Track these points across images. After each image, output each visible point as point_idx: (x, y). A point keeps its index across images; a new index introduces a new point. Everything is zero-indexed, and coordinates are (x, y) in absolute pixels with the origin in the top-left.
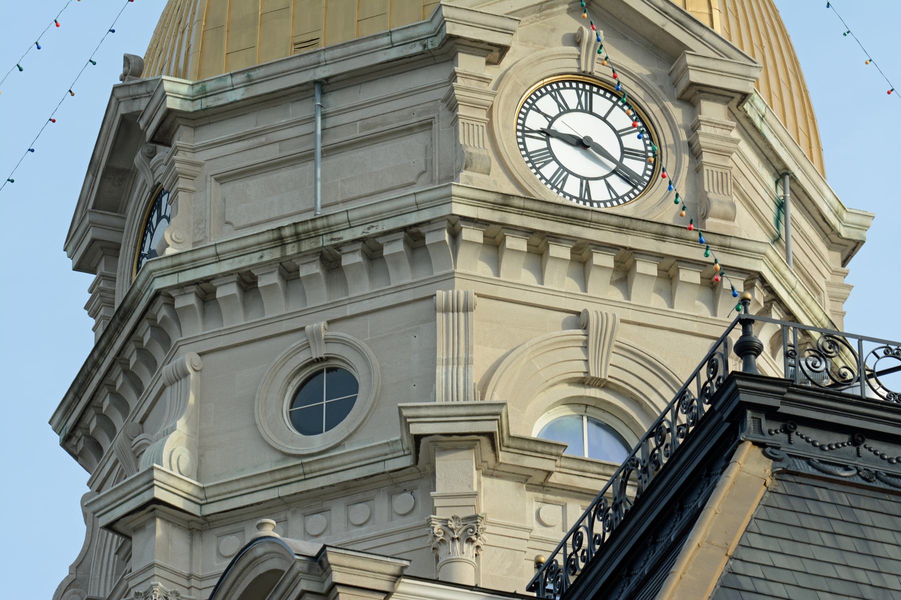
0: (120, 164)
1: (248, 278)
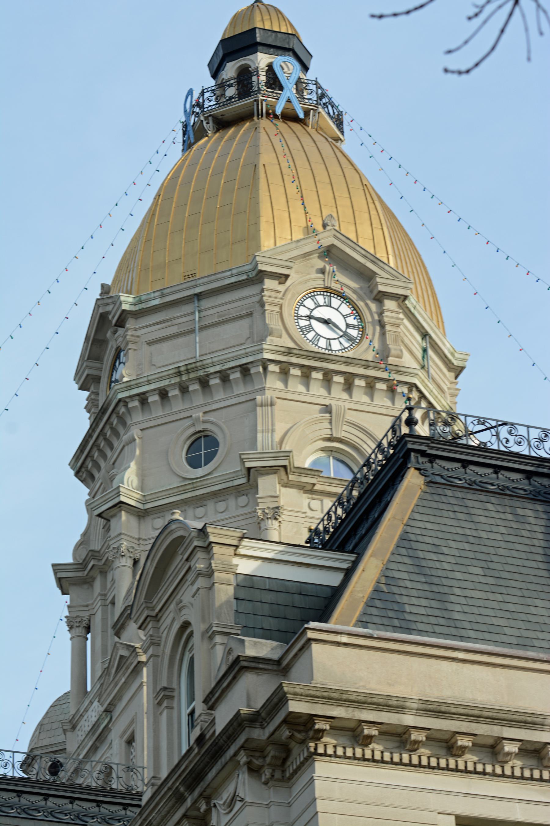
0: (100, 337)
1: (164, 392)
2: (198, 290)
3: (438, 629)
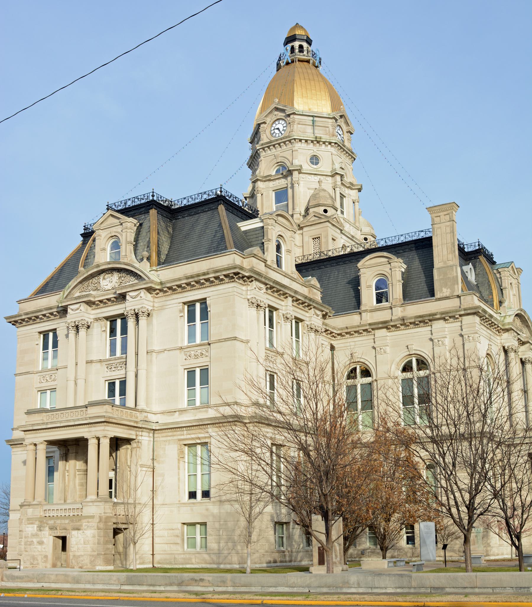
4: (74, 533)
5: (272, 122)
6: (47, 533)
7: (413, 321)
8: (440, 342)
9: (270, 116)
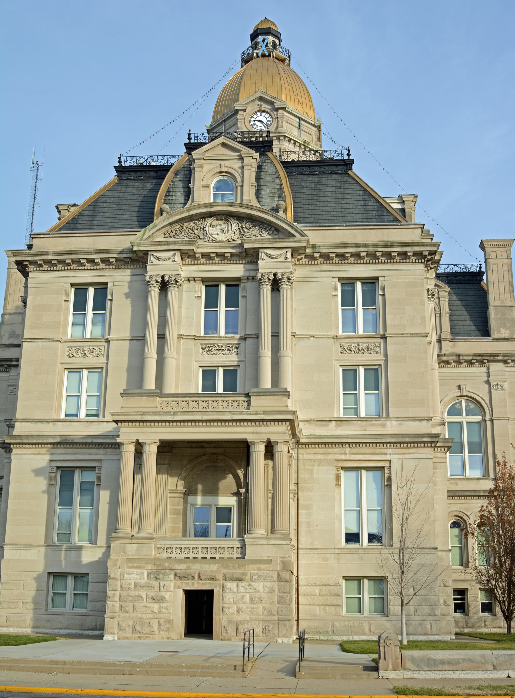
2: (224, 119)
3: (84, 227)
4: (231, 585)
5: (253, 112)
6: (172, 585)
7: (470, 358)
8: (499, 387)
9: (251, 104)
